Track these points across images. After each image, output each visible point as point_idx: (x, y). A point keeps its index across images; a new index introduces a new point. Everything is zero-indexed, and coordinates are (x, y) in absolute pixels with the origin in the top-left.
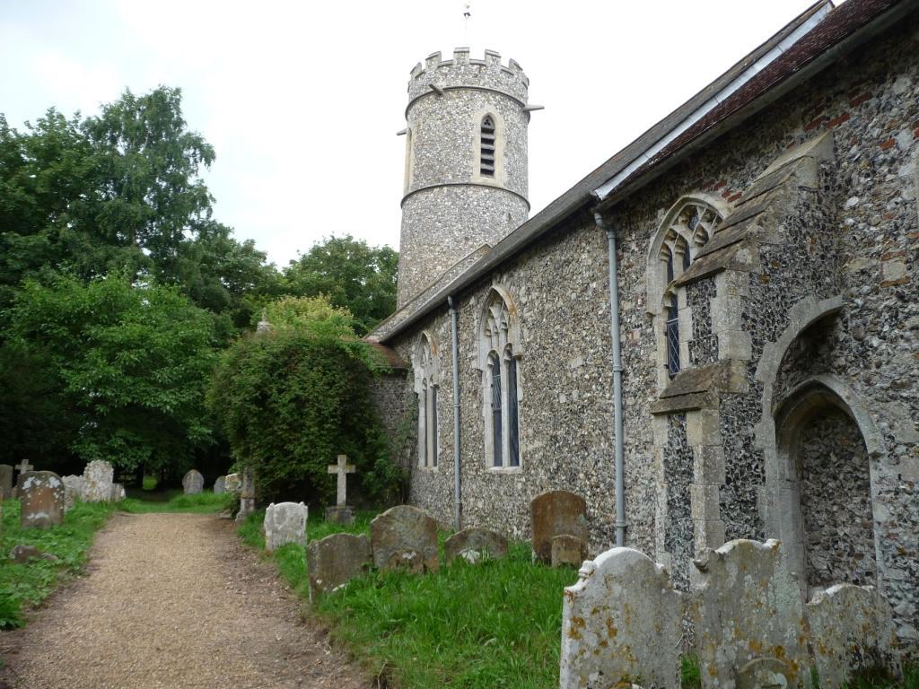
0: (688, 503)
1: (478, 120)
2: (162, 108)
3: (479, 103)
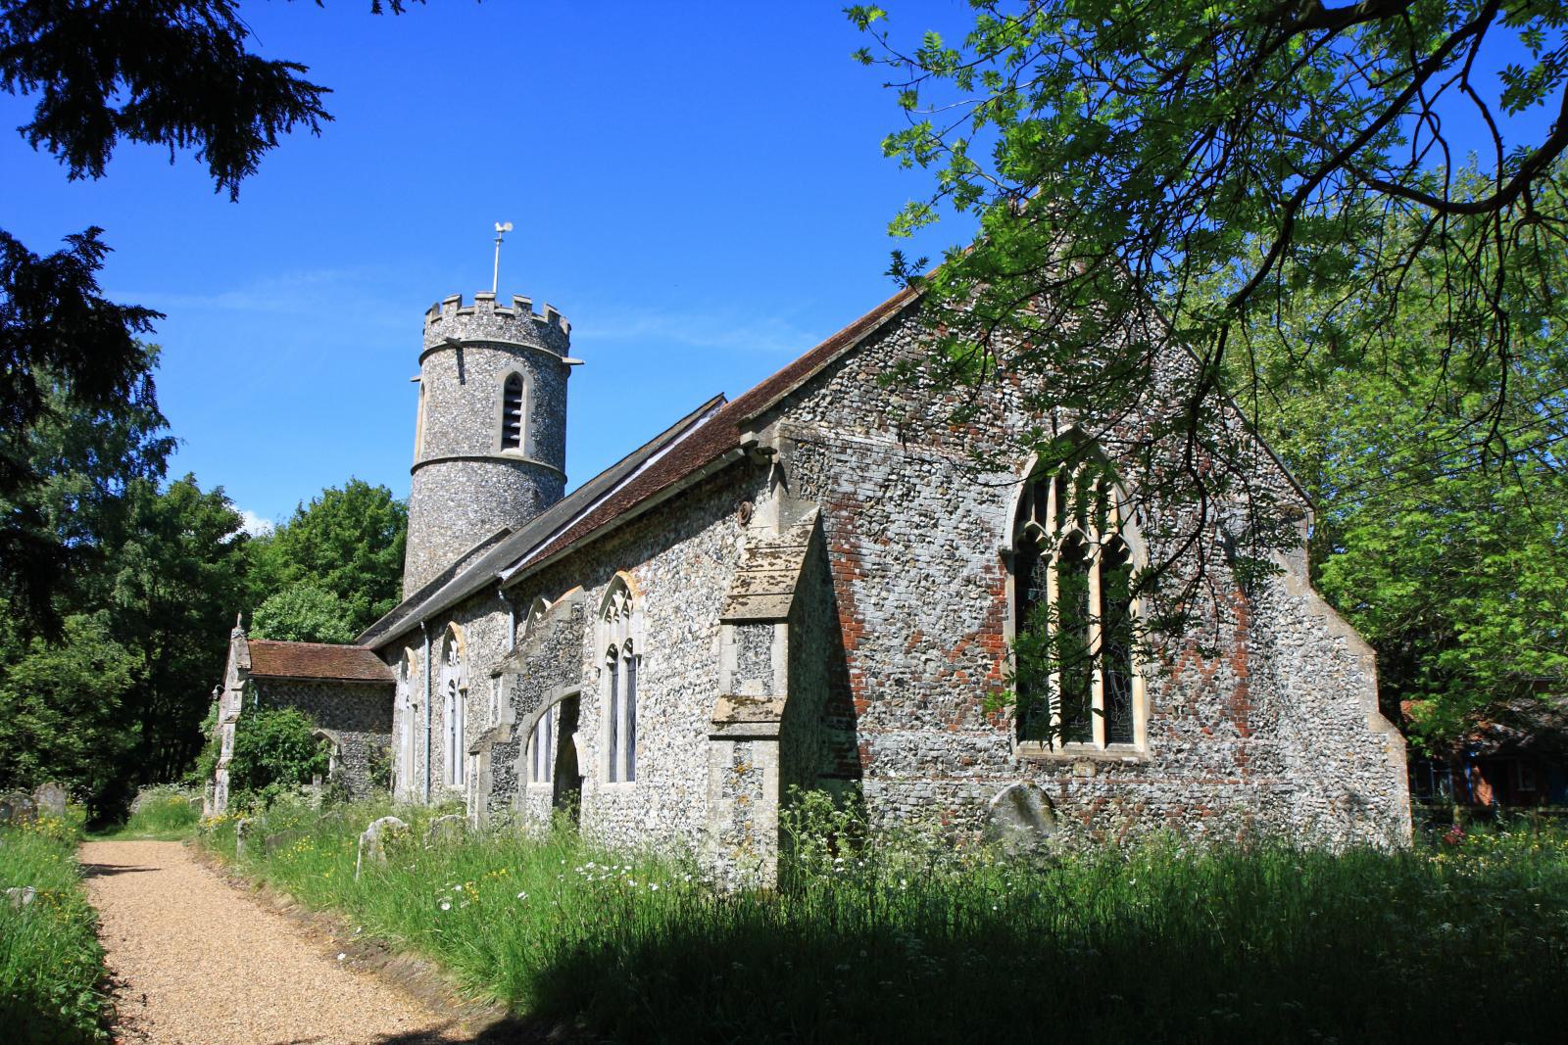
0: (783, 835)
1: (500, 381)
2: (98, 171)
3: (503, 361)
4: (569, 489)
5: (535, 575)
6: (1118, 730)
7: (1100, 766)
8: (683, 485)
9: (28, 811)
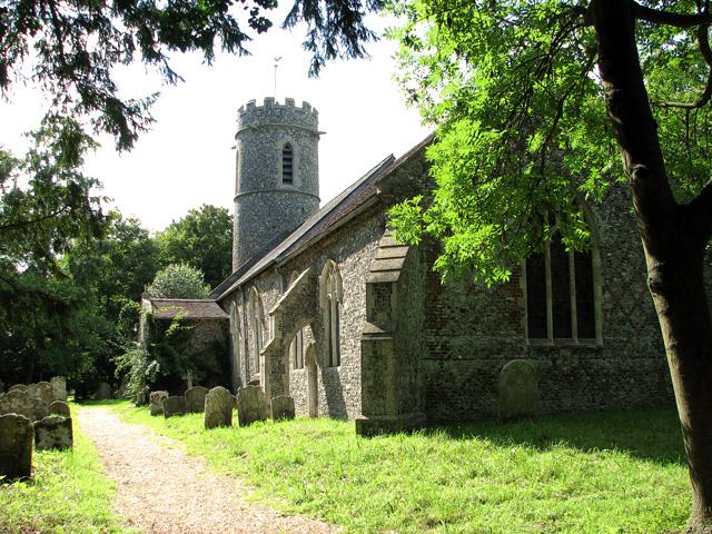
4: (321, 205)
6: (588, 330)
7: (575, 350)
9: (39, 225)
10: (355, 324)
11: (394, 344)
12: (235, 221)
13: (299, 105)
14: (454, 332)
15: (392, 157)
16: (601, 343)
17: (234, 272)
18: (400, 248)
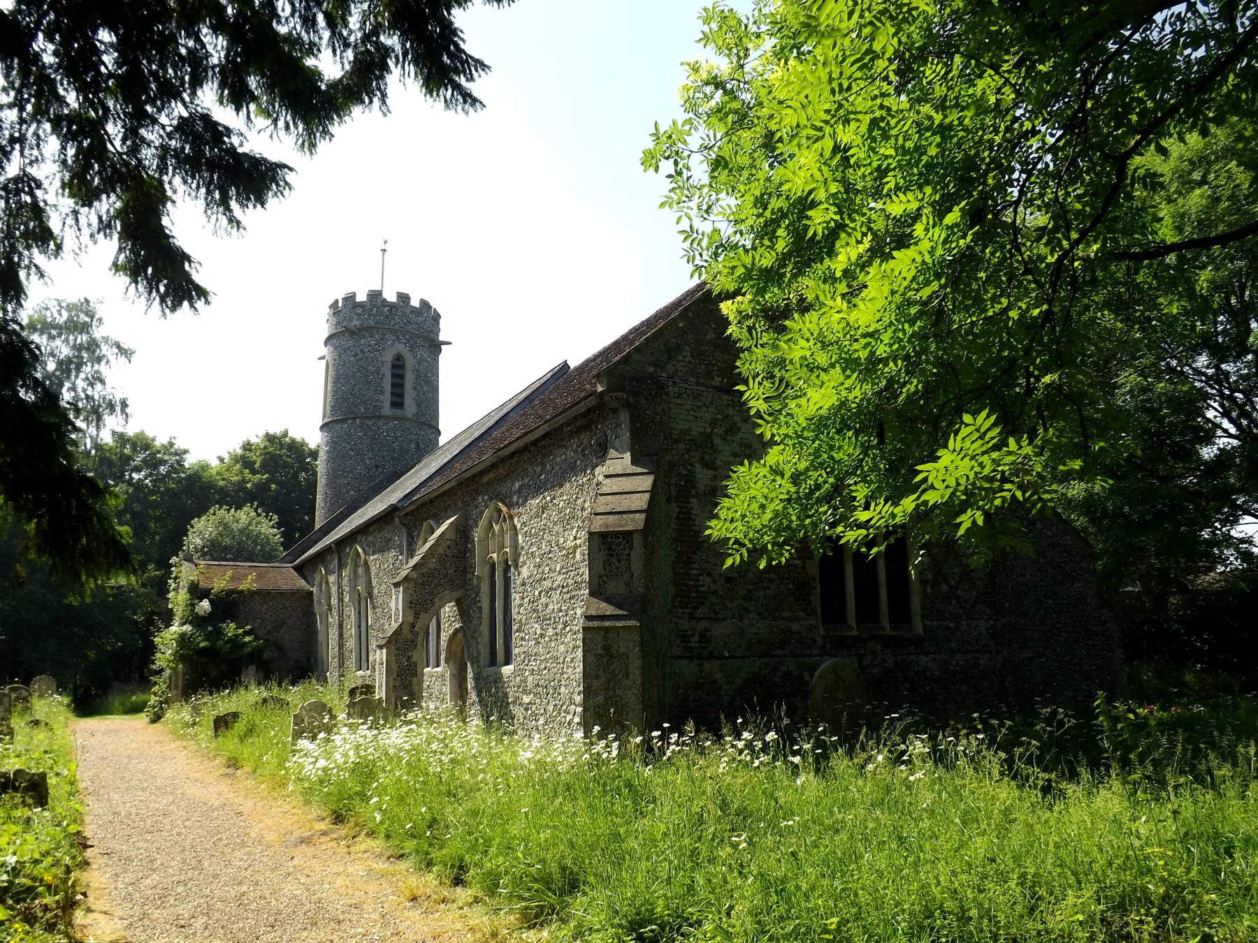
4: (442, 440)
5: (424, 504)
6: (901, 612)
8: (546, 428)
10: (543, 600)
11: (641, 636)
12: (321, 465)
13: (415, 303)
14: (716, 613)
15: (565, 365)
16: (920, 630)
17: (317, 526)
18: (624, 479)
